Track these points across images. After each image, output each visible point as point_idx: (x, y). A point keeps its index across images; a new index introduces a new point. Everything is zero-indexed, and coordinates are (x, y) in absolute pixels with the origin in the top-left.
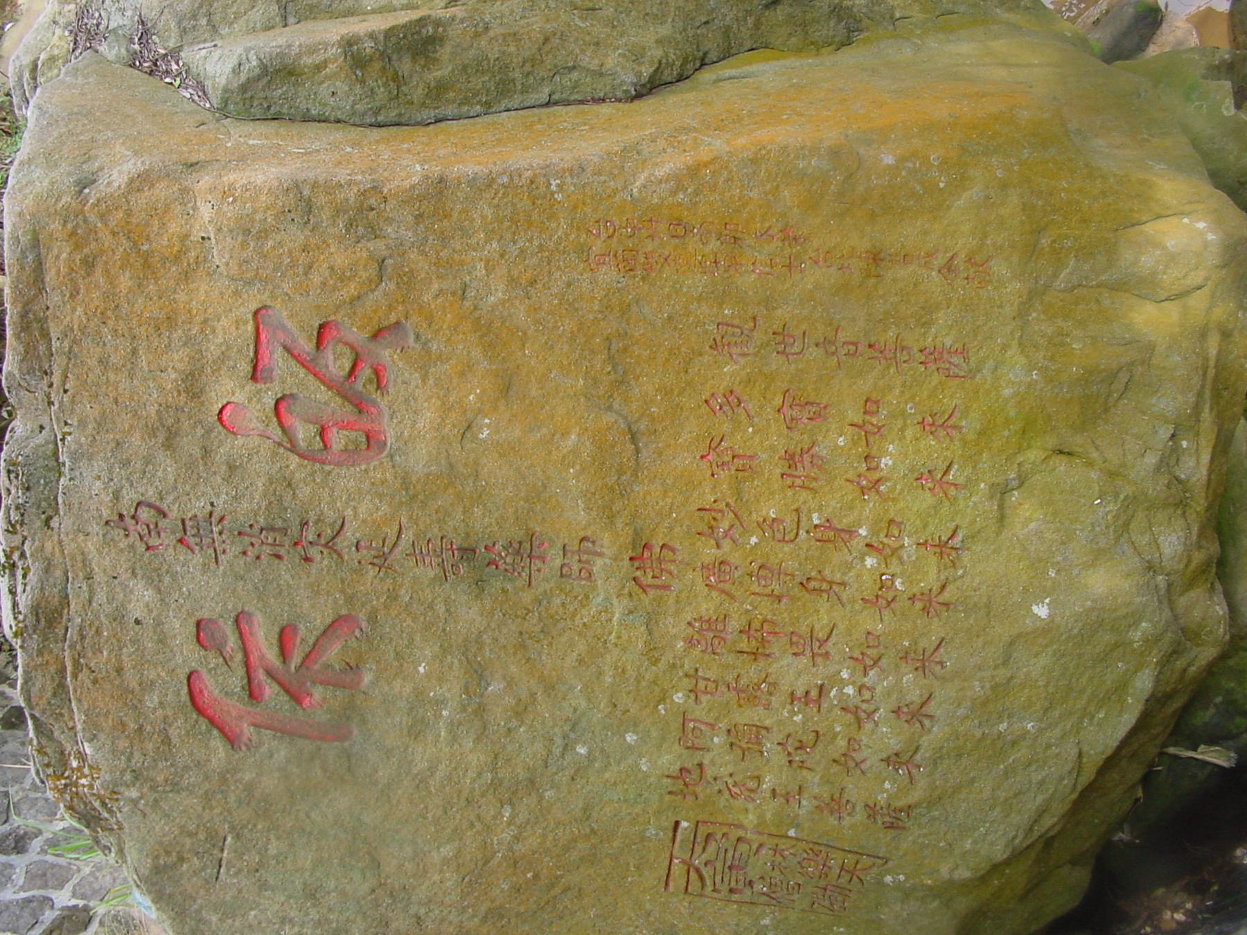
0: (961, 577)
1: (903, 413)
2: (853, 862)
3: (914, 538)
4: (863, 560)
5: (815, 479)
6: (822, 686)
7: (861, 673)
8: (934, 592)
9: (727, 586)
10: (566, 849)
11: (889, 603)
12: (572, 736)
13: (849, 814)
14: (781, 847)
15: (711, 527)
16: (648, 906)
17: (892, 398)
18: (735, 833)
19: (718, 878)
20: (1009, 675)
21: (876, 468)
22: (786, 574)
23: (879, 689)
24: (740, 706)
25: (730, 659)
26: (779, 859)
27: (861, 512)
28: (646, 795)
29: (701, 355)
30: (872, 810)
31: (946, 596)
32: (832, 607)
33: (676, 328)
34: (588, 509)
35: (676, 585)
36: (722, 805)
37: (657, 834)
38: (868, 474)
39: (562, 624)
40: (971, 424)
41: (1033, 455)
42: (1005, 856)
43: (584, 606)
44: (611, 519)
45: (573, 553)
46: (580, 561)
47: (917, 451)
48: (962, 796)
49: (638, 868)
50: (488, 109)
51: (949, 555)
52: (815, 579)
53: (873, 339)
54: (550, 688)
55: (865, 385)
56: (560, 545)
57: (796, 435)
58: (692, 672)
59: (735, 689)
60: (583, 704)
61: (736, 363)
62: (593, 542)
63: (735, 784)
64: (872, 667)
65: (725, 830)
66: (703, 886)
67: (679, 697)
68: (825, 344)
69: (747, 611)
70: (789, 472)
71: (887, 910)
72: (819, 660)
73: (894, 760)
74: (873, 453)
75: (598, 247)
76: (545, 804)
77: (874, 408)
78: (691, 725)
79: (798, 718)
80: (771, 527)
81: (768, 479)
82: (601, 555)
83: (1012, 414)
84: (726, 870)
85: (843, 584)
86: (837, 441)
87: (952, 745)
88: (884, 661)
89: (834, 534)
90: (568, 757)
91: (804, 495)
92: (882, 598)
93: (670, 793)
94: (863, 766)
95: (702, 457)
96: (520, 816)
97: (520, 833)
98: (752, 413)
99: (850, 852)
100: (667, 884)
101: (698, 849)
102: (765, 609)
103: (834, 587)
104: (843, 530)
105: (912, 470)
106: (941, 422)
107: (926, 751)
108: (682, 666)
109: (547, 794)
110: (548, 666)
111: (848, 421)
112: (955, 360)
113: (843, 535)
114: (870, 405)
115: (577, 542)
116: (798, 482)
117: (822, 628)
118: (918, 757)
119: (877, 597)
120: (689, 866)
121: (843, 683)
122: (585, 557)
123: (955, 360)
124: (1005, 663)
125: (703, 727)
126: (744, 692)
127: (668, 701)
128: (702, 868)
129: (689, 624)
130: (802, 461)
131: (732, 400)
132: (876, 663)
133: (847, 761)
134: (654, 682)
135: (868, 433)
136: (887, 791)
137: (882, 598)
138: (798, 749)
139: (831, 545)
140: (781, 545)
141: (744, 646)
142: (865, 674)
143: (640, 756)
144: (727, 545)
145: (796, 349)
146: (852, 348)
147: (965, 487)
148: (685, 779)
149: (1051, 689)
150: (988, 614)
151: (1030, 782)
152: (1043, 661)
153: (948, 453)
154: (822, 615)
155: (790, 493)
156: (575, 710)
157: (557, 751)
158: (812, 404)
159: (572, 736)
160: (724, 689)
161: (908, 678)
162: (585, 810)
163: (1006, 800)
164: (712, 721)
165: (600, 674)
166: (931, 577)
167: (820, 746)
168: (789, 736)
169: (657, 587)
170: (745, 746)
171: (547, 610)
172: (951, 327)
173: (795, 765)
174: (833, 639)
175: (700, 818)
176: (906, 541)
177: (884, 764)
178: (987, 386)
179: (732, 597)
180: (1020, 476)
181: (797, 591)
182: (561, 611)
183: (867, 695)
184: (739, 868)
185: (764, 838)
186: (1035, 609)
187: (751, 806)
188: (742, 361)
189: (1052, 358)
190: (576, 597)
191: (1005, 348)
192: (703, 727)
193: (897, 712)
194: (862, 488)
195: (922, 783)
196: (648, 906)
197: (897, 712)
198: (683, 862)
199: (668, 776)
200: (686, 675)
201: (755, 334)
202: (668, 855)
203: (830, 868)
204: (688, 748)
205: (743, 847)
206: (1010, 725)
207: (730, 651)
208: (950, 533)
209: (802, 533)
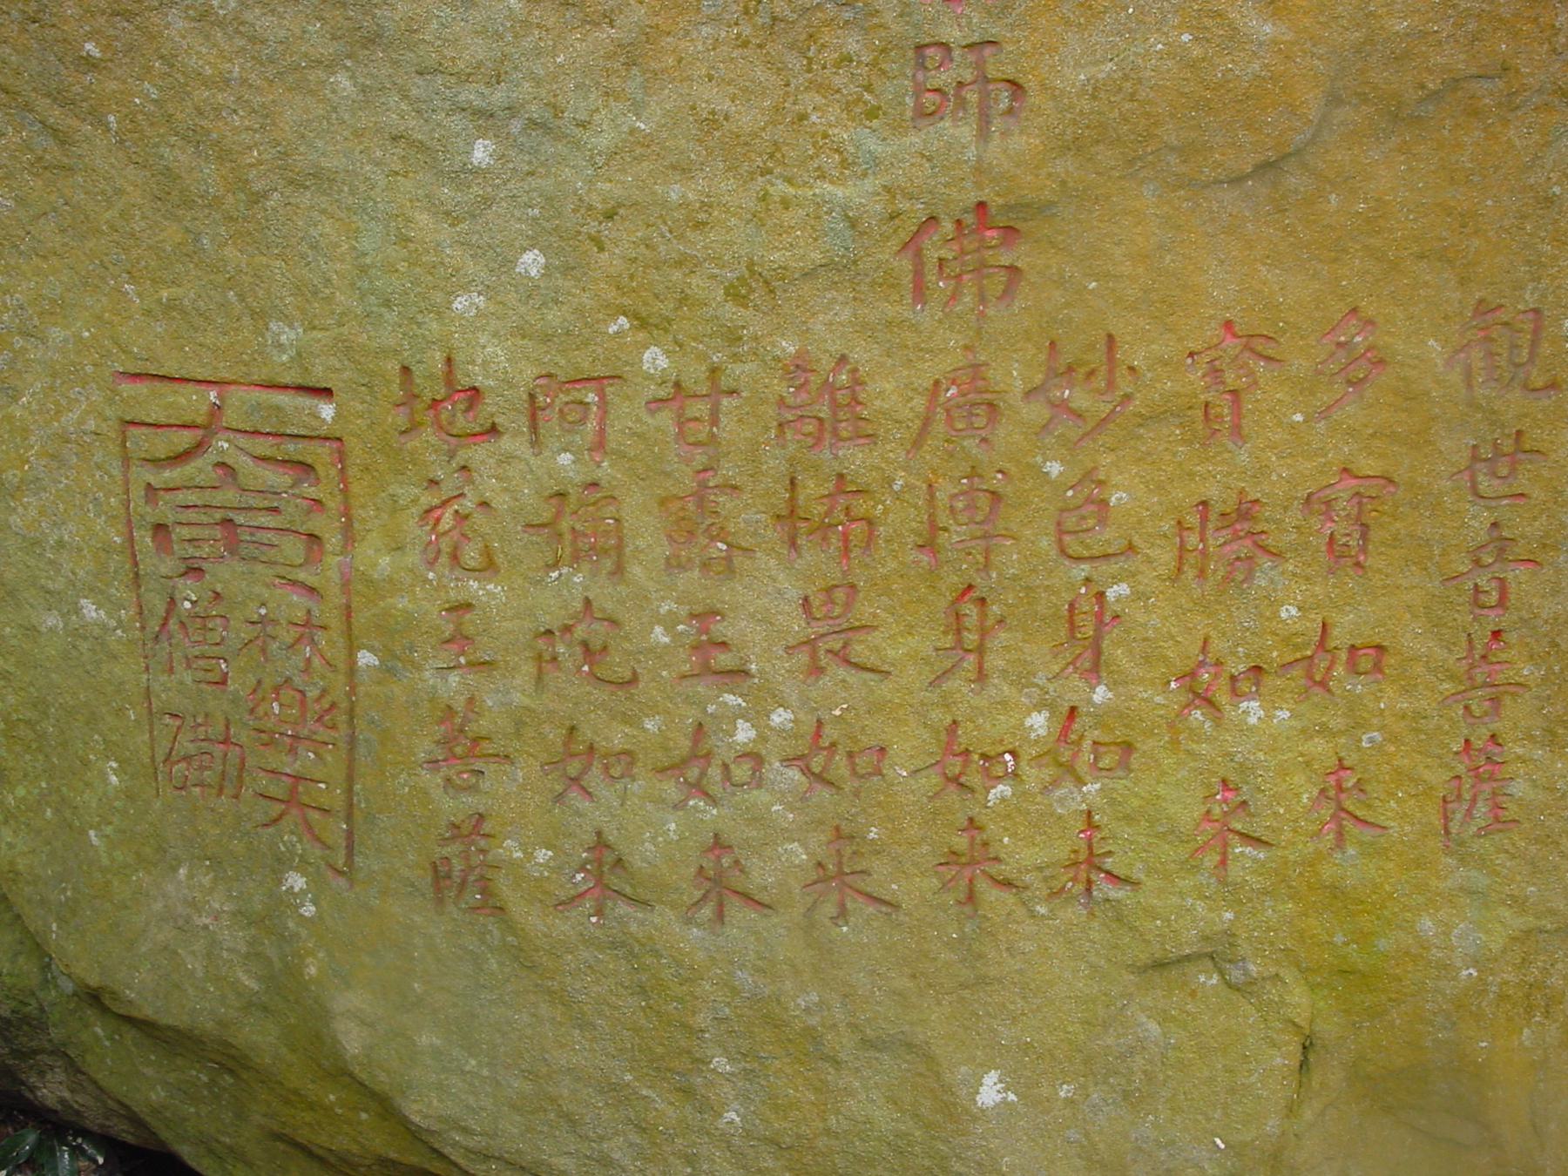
0: (1032, 915)
1: (1360, 725)
2: (325, 802)
3: (1099, 802)
4: (1038, 707)
5: (1202, 573)
6: (746, 673)
7: (791, 752)
8: (994, 869)
9: (939, 427)
10: (195, 138)
11: (955, 780)
12: (516, 126)
13: (448, 780)
14: (322, 638)
15: (1070, 369)
16: (57, 334)
17: (1390, 699)
18: (328, 527)
19: (192, 498)
20: (842, 1056)
21: (1235, 693)
22: (987, 553)
23: (760, 796)
24: (663, 502)
25: (774, 462)
26: (288, 635)
27: (1142, 680)
28: (391, 316)
29: (1463, 282)
30: (474, 829)
31: (990, 894)
32: (926, 661)
33: (1524, 217)
34: (1094, 91)
35: (927, 316)
36: (394, 489)
37: (280, 347)
38: (1224, 681)
39: (795, 62)
40: (1351, 866)
41: (1298, 999)
42: (416, 1119)
43: (847, 108)
44: (1076, 146)
45: (980, 65)
46: (960, 85)
47: (1283, 772)
48: (544, 1010)
49: (170, 307)
51: (1074, 880)
52: (983, 616)
53: (1512, 637)
54: (630, 56)
55: (1413, 639)
56: (994, 31)
57: (1294, 517)
58: (725, 382)
59: (703, 486)
60: (604, 141)
61: (1449, 363)
62: (1010, 111)
63: (461, 518)
64: (807, 771)
65: (333, 504)
66: (156, 462)
67: (655, 359)
68: (1500, 542)
69: (890, 481)
70: (1213, 516)
71: (206, 881)
72: (803, 658)
73: (605, 862)
74: (1269, 681)
76: (314, 76)
77: (1365, 663)
78: (591, 397)
79: (660, 635)
80: (1089, 500)
81: (1191, 475)
82: (983, 134)
83: (1382, 944)
84: (218, 515)
85: (981, 676)
86: (1290, 603)
87: (666, 974)
88: (825, 793)
89: (1088, 637)
90: (457, 123)
91: (1165, 557)
92: (962, 762)
93: (406, 370)
94: (574, 794)
95: (1228, 325)
96: (268, 21)
97: (221, 24)
98: (1336, 415)
99: (349, 791)
100: (137, 376)
101: (263, 446)
102: (898, 519)
103: (972, 658)
104: (1098, 653)
105: (1243, 768)
106: (1348, 805)
107: (642, 923)
108: (736, 358)
109: (343, 81)
110: (683, 44)
111: (1334, 616)
112: (1482, 808)
113: (1088, 654)
114: (1372, 656)
115: (1010, 72)
116: (1193, 540)
117: (877, 649)
118: (623, 908)
119: (967, 752)
120: (211, 425)
121: (757, 715)
122: (972, 96)
123: (1482, 808)
124: (867, 1043)
125: (592, 425)
126: (700, 505)
127: (641, 336)
128: (211, 457)
129: (843, 359)
130: (1236, 537)
131: (1361, 368)
132: (820, 778)
133: (576, 761)
134: (684, 300)
135: (1313, 664)
136: (529, 856)
137: (962, 762)
138: (587, 643)
139: (1063, 633)
140: (1052, 528)
141: (810, 488)
142: (788, 761)
143: (488, 291)
144: (1036, 412)
145: (1485, 484)
146: (1494, 598)
147: (1223, 882)
148: (450, 404)
149: (821, 1143)
150: (964, 986)
151: (602, 1138)
152: (884, 1117)
153: (1287, 835)
154: (904, 642)
155: (1167, 526)
156: (583, 125)
157: (469, 95)
158: (1364, 536)
159: (516, 126)
160: (700, 459)
161: (799, 854)
162: (317, 174)
163: (553, 1100)
164: (612, 445)
165: (684, 170)
166: (1022, 854)
167: (601, 694)
168: (613, 622)
169: (918, 275)
170: (565, 525)
171: (829, 23)
172: (1553, 790)
173: (541, 644)
174: (853, 677)
175: (351, 443)
176: (1092, 788)
177: (590, 839)
178: (1434, 882)
179: (917, 443)
180: (1253, 982)
181: (952, 581)
182: (830, 56)
183: (741, 772)
184: (233, 545)
185: (335, 597)
186: (991, 1078)
187: (413, 558)
188: (1456, 377)
189: (1502, 997)
190: (868, 88)
191: (1518, 903)
192: (592, 425)
193: (719, 844)
194: (1193, 674)
195: (563, 926)
196: (57, 334)
197: (719, 844)
198: (216, 410)
199: (449, 360)
200: (714, 370)
201: (1518, 393)
202: (226, 375)
203: (292, 751)
204: (532, 397)
205: (293, 549)
206: (729, 1077)
207: (792, 461)
208: (1120, 871)
209: (1084, 570)
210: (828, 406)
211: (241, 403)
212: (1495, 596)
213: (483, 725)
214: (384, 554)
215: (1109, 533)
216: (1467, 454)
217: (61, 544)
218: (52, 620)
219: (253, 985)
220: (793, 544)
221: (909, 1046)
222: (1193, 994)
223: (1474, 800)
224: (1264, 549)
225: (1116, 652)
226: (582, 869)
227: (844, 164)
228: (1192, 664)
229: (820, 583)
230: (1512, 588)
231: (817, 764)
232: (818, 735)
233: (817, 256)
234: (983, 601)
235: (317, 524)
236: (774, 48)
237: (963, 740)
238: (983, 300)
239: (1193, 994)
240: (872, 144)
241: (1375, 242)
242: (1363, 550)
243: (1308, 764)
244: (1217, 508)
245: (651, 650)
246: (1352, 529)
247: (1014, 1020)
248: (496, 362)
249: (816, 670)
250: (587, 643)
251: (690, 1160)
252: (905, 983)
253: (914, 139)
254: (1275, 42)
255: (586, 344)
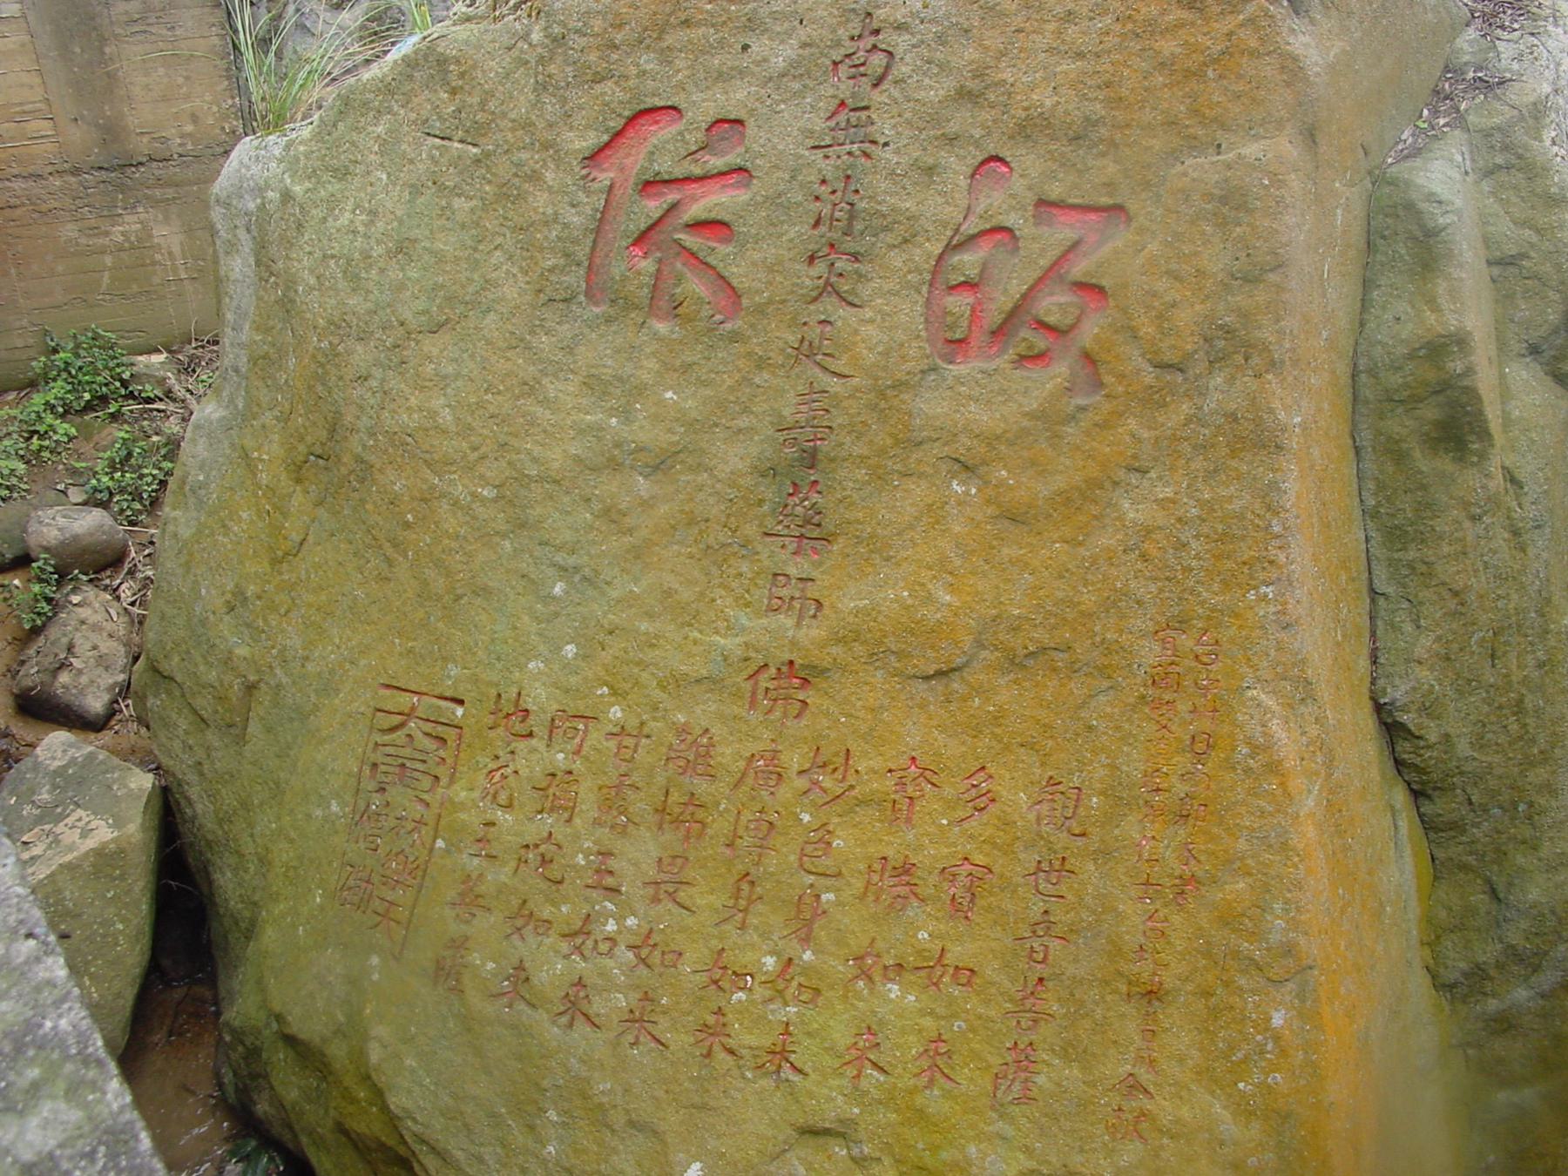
0: (744, 1077)
1: (955, 1016)
4: (771, 953)
5: (877, 900)
6: (619, 891)
7: (631, 942)
8: (725, 1040)
9: (750, 781)
11: (716, 982)
12: (577, 578)
15: (824, 765)
23: (609, 963)
25: (660, 780)
26: (410, 826)
27: (832, 954)
28: (499, 666)
29: (1043, 764)
30: (459, 944)
32: (716, 911)
34: (857, 612)
35: (755, 717)
37: (449, 677)
40: (934, 1101)
43: (736, 600)
46: (792, 598)
47: (903, 1031)
50: (1370, 514)
52: (751, 892)
53: (1050, 984)
54: (637, 553)
55: (991, 970)
56: (814, 574)
57: (934, 879)
60: (615, 594)
62: (814, 616)
63: (504, 777)
64: (637, 956)
66: (383, 731)
67: (616, 712)
73: (521, 974)
75: (1186, 641)
78: (581, 726)
82: (798, 625)
89: (806, 919)
90: (551, 572)
91: (859, 884)
97: (462, 508)
98: (966, 825)
99: (412, 914)
100: (388, 686)
101: (428, 727)
102: (719, 826)
104: (811, 930)
105: (881, 1022)
108: (654, 719)
109: (507, 544)
111: (949, 945)
112: (1017, 1087)
114: (967, 975)
115: (816, 595)
116: (876, 878)
118: (522, 1006)
119: (725, 968)
120: (409, 714)
123: (1017, 1087)
125: (577, 740)
128: (405, 731)
129: (707, 730)
131: (982, 801)
133: (524, 918)
135: (929, 969)
136: (484, 964)
137: (724, 974)
141: (675, 797)
142: (630, 947)
143: (546, 661)
144: (802, 783)
148: (514, 716)
153: (899, 1070)
154: (707, 897)
155: (862, 866)
157: (559, 558)
158: (972, 901)
159: (577, 578)
160: (624, 768)
165: (650, 616)
166: (745, 1037)
167: (544, 885)
168: (560, 847)
169: (754, 693)
170: (551, 791)
172: (1059, 1085)
173: (523, 851)
174: (676, 910)
175: (466, 730)
177: (515, 962)
179: (736, 786)
182: (732, 571)
184: (402, 777)
187: (476, 794)
188: (1032, 816)
190: (748, 591)
191: (1028, 1151)
192: (577, 740)
193: (580, 983)
196: (363, 662)
197: (580, 983)
198: (413, 708)
200: (642, 724)
202: (424, 690)
205: (426, 782)
206: (554, 1124)
207: (669, 780)
210: (696, 755)
211: (425, 705)
212: (1042, 955)
213: (482, 889)
214: (465, 793)
215: (829, 862)
216: (1035, 864)
217: (333, 770)
218: (319, 813)
219: (342, 1019)
220: (660, 828)
221: (655, 1133)
222: (829, 1157)
223: (1013, 1080)
224: (915, 894)
225: (821, 934)
226: (508, 979)
227: (728, 628)
228: (863, 951)
229: (670, 852)
230: (1051, 952)
231: (644, 952)
232: (648, 936)
233: (704, 673)
234: (752, 883)
235: (441, 771)
236: (705, 562)
237: (724, 961)
238: (785, 715)
239: (829, 1157)
240: (744, 621)
241: (998, 731)
242: (970, 909)
243: (920, 1031)
244: (893, 863)
245: (574, 866)
246: (967, 893)
247: (719, 1137)
248: (540, 698)
249: (656, 900)
250: (543, 858)
251: (524, 1170)
252: (660, 1094)
253: (764, 621)
254: (949, 605)
255: (586, 696)
